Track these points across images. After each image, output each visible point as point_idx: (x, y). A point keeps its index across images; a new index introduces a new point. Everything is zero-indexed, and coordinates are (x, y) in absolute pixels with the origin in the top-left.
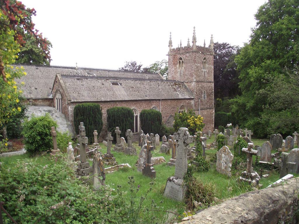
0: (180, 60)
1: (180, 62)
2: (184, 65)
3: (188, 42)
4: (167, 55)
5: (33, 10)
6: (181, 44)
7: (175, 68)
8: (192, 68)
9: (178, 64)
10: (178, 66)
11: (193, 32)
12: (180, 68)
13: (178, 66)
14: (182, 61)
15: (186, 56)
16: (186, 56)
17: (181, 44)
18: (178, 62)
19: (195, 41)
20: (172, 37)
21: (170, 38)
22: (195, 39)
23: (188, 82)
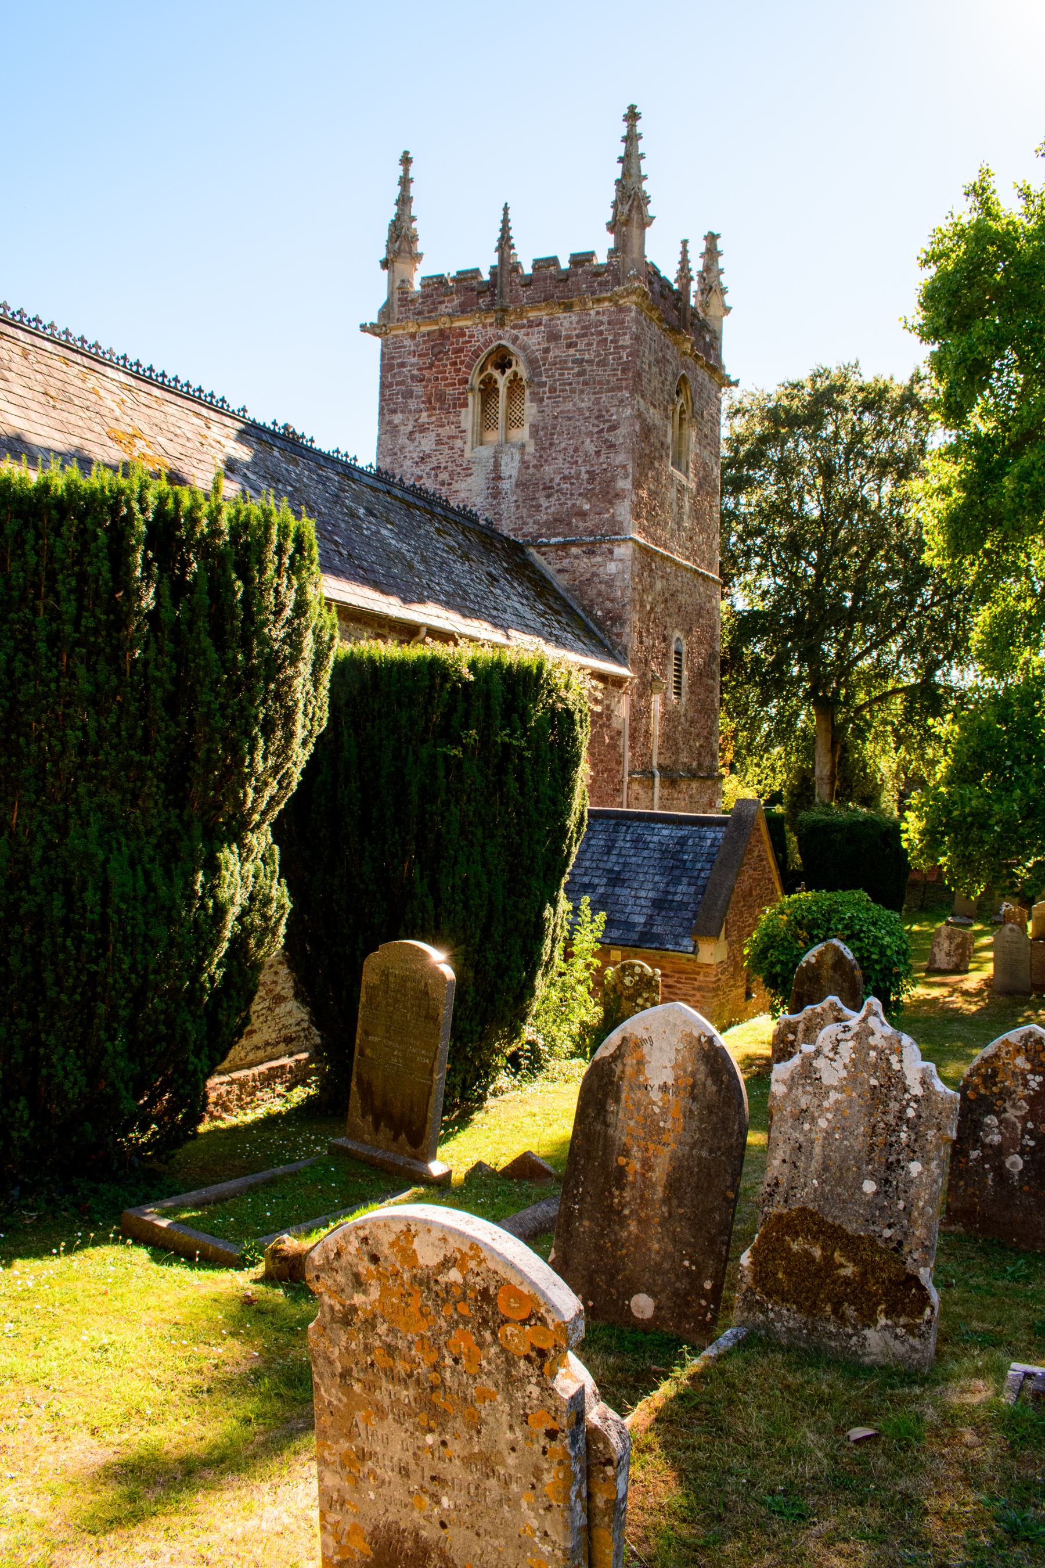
0: (496, 374)
1: (489, 389)
2: (530, 410)
3: (684, 253)
4: (653, 218)
5: (706, 238)
6: (505, 243)
7: (446, 431)
8: (613, 428)
9: (473, 401)
10: (469, 417)
11: (623, 130)
12: (493, 437)
13: (469, 417)
14: (515, 382)
15: (553, 336)
16: (553, 336)
17: (505, 243)
18: (475, 380)
19: (635, 215)
20: (414, 190)
21: (404, 201)
22: (189, 1473)
23: (573, 543)
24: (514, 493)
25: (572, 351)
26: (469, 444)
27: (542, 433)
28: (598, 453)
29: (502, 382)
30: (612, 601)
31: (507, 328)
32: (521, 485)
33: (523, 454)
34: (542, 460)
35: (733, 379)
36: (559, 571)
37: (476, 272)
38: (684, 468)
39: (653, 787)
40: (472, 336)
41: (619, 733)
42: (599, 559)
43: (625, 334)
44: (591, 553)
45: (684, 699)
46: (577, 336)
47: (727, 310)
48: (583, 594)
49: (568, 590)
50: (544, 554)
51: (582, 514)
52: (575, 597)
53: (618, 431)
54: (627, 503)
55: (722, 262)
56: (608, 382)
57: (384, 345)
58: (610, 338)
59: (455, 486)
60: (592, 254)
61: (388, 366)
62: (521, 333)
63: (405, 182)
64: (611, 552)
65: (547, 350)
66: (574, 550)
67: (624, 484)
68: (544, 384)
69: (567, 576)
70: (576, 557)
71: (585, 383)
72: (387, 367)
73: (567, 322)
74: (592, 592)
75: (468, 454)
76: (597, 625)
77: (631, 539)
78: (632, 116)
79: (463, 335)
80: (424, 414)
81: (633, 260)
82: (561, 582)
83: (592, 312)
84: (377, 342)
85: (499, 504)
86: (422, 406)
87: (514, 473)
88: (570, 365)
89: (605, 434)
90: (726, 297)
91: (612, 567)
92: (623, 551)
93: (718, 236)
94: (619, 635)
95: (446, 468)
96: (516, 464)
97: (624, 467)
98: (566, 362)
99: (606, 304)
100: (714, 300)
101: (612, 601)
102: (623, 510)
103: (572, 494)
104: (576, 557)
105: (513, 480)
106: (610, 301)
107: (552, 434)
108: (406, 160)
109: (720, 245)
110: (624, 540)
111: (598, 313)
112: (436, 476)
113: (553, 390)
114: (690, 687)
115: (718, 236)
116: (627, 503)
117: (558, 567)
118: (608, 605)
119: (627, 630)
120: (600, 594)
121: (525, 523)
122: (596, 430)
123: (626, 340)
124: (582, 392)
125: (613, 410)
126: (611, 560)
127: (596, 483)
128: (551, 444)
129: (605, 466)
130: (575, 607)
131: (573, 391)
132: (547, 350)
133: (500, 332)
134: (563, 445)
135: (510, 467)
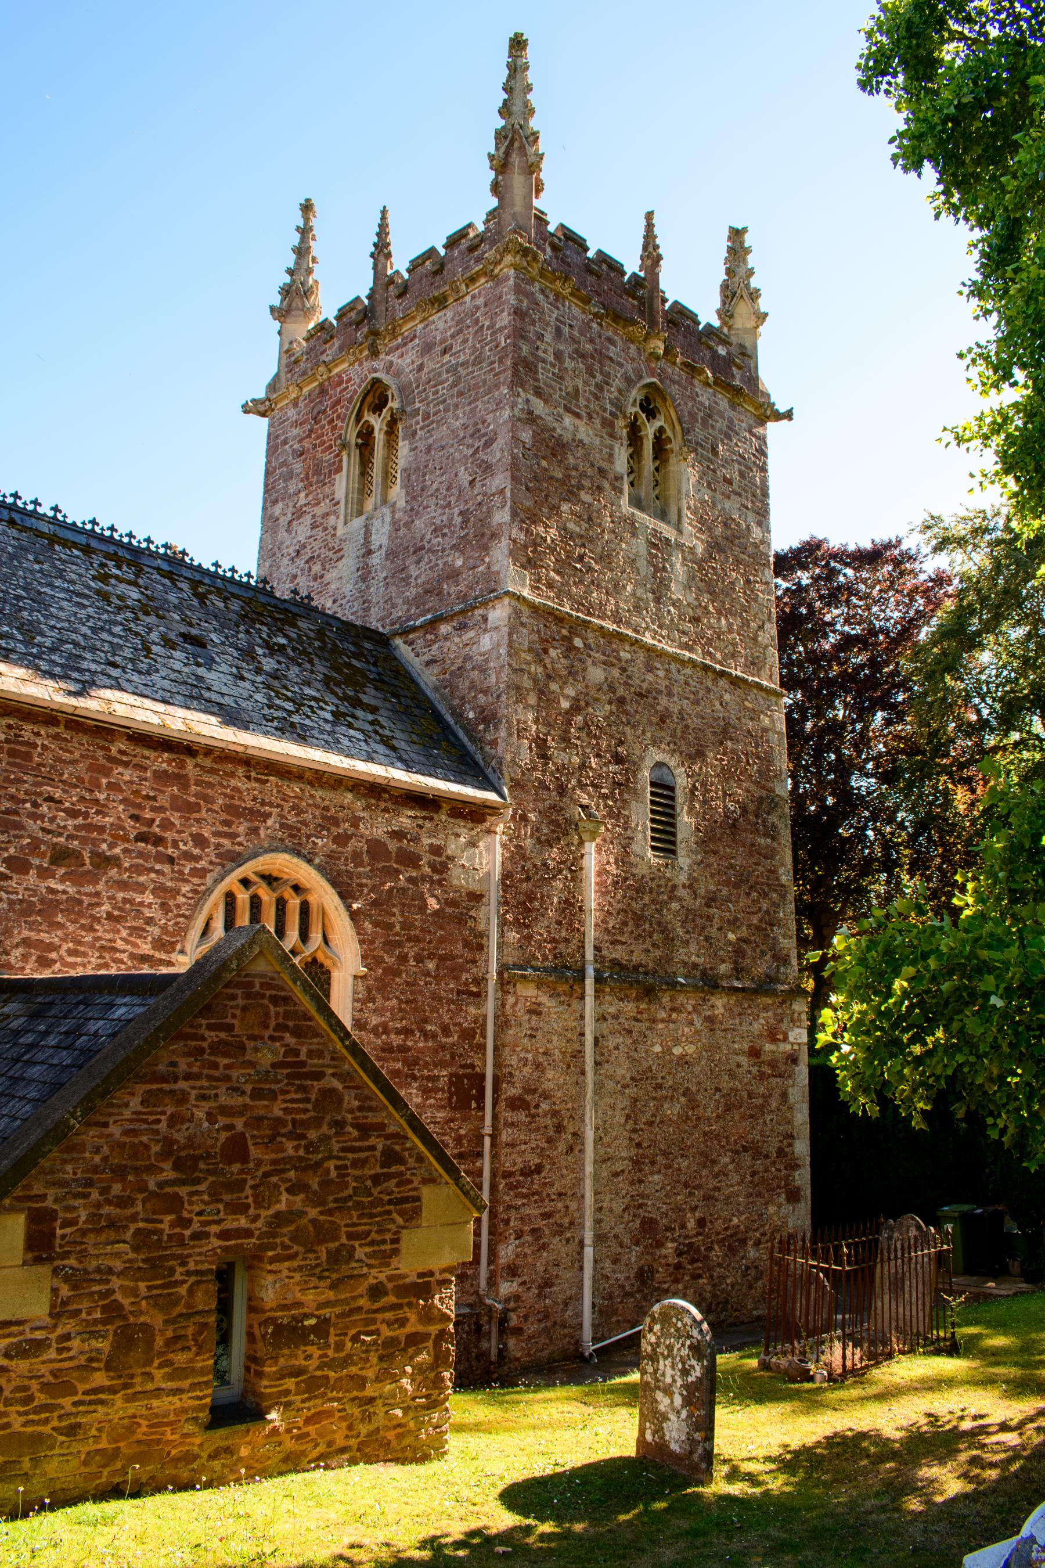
8: (488, 444)
9: (350, 462)
17: (381, 250)
21: (302, 251)
24: (383, 568)
25: (447, 357)
26: (342, 517)
27: (413, 477)
28: (472, 482)
29: (378, 423)
30: (485, 692)
31: (382, 356)
32: (391, 555)
33: (393, 512)
34: (412, 512)
35: (782, 408)
36: (428, 664)
37: (358, 299)
38: (673, 516)
39: (582, 998)
40: (349, 380)
41: (476, 897)
42: (471, 634)
43: (502, 311)
44: (462, 627)
45: (684, 860)
46: (453, 336)
47: (762, 317)
48: (453, 688)
49: (436, 689)
50: (411, 644)
51: (454, 575)
52: (443, 697)
53: (495, 445)
54: (504, 544)
55: (752, 260)
56: (485, 381)
57: (271, 425)
58: (487, 323)
59: (328, 577)
60: (470, 225)
61: (274, 445)
62: (392, 358)
63: (305, 232)
64: (485, 619)
65: (420, 368)
66: (444, 629)
67: (502, 516)
68: (417, 412)
69: (436, 669)
70: (446, 638)
71: (461, 394)
72: (272, 450)
73: (442, 322)
74: (463, 685)
75: (339, 532)
76: (467, 732)
77: (507, 593)
78: (518, 44)
79: (340, 383)
80: (302, 495)
81: (514, 216)
82: (428, 679)
83: (468, 298)
84: (262, 424)
85: (368, 587)
86: (301, 485)
87: (385, 541)
88: (445, 376)
89: (481, 455)
90: (761, 301)
91: (486, 642)
92: (499, 614)
93: (745, 230)
94: (494, 743)
95: (319, 556)
96: (387, 528)
97: (502, 492)
98: (440, 374)
99: (483, 280)
100: (742, 309)
101: (485, 692)
102: (500, 556)
103: (444, 550)
104: (446, 638)
105: (383, 551)
106: (485, 274)
107: (425, 475)
108: (307, 208)
109: (748, 240)
110: (497, 598)
111: (473, 297)
112: (310, 569)
113: (427, 416)
114: (700, 843)
115: (745, 230)
116: (504, 544)
117: (426, 658)
118: (482, 699)
119: (503, 733)
120: (472, 686)
121: (394, 606)
122: (471, 451)
123: (505, 319)
124: (456, 406)
125: (489, 418)
126: (486, 631)
127: (471, 524)
128: (422, 490)
129: (480, 498)
130: (443, 711)
131: (446, 410)
132: (420, 368)
133: (375, 364)
134: (435, 486)
135: (381, 536)
